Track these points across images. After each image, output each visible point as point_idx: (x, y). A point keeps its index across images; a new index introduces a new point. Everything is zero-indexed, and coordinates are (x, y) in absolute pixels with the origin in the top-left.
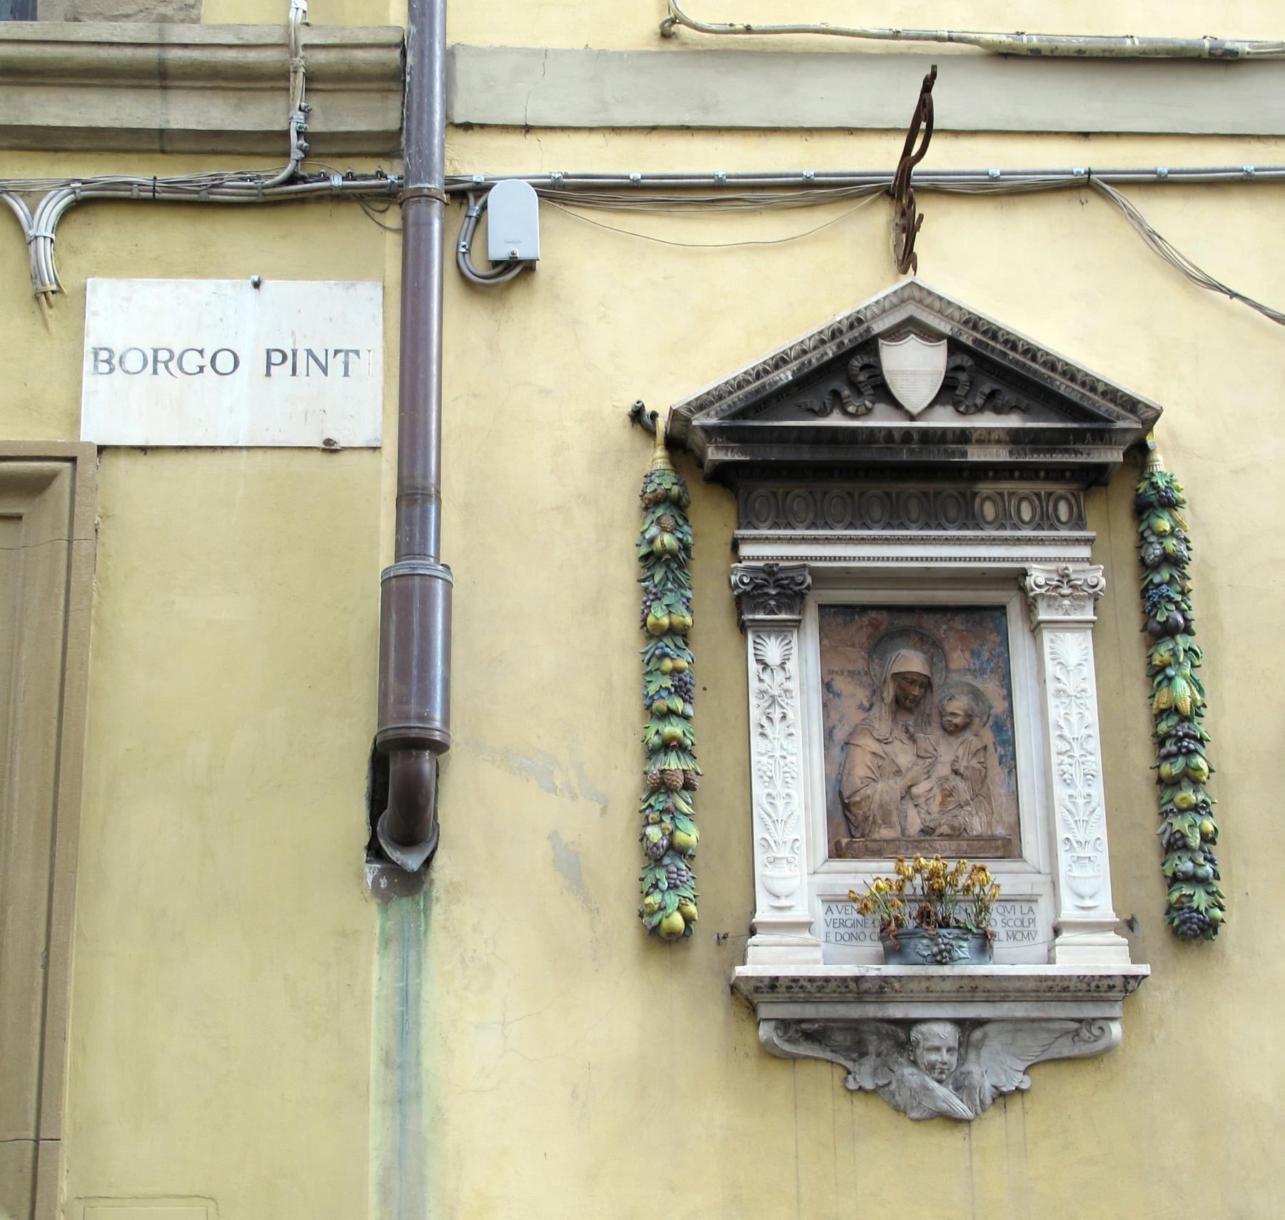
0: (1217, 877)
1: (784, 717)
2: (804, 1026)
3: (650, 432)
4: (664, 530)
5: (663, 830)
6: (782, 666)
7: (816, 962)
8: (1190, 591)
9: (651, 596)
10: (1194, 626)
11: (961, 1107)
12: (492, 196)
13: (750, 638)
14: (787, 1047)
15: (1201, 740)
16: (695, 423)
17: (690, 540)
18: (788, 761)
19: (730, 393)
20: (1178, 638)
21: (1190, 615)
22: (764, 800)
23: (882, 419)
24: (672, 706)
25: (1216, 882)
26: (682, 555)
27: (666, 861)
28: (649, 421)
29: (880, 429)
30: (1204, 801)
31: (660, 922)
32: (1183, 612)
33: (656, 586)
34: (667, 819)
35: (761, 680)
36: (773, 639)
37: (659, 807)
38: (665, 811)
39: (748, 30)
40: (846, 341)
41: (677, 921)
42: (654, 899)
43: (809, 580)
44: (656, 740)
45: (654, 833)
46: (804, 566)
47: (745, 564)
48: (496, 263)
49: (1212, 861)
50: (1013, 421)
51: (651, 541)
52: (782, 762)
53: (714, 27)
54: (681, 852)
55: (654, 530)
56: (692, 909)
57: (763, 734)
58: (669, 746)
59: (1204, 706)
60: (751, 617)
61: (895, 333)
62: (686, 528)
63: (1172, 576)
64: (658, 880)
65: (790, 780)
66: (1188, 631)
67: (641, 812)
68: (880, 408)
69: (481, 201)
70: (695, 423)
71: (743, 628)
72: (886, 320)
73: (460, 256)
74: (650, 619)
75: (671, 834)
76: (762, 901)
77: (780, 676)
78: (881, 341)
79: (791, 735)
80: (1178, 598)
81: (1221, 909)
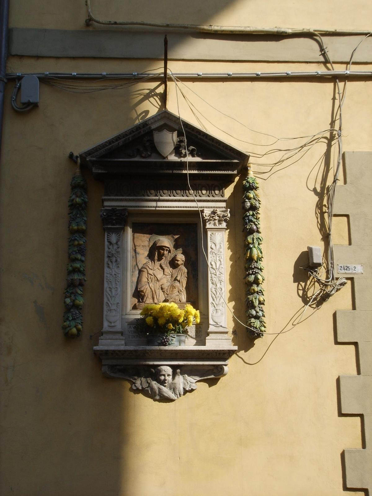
0: (264, 316)
1: (116, 261)
2: (118, 367)
3: (76, 162)
4: (77, 196)
5: (71, 299)
6: (117, 243)
7: (122, 345)
8: (259, 218)
9: (73, 219)
10: (260, 230)
11: (171, 395)
12: (23, 81)
13: (106, 234)
14: (112, 375)
15: (261, 269)
16: (87, 159)
17: (86, 200)
18: (117, 276)
19: (100, 149)
20: (254, 234)
21: (259, 226)
22: (108, 289)
23: (154, 159)
24: (77, 257)
25: (263, 318)
26: (83, 205)
27: (72, 310)
28: (75, 159)
29: (152, 162)
30: (260, 290)
31: (68, 331)
32: (256, 225)
33: (73, 216)
34: (73, 296)
35: (109, 248)
36: (114, 234)
37: (71, 292)
38: (72, 293)
39: (115, 23)
40: (142, 132)
41: (74, 330)
42: (68, 323)
43: (127, 214)
44: (70, 268)
45: (68, 301)
46: (125, 209)
47: (105, 208)
48: (24, 104)
49: (262, 311)
50: (198, 159)
51: (73, 200)
52: (115, 276)
53: (104, 22)
54: (77, 307)
55: (74, 197)
56: (80, 327)
57: (108, 267)
58: (75, 271)
59: (262, 257)
60: (106, 227)
61: (160, 129)
62: (86, 196)
63: (253, 213)
64: (68, 317)
65: (118, 283)
66: (258, 232)
67: (64, 293)
68: (154, 155)
69: (20, 82)
70: (87, 159)
71: (104, 230)
72: (156, 124)
73: (13, 102)
74: (71, 227)
75: (74, 301)
76: (106, 324)
77: (115, 247)
78: (154, 132)
79: (118, 267)
80: (255, 220)
81: (265, 327)
